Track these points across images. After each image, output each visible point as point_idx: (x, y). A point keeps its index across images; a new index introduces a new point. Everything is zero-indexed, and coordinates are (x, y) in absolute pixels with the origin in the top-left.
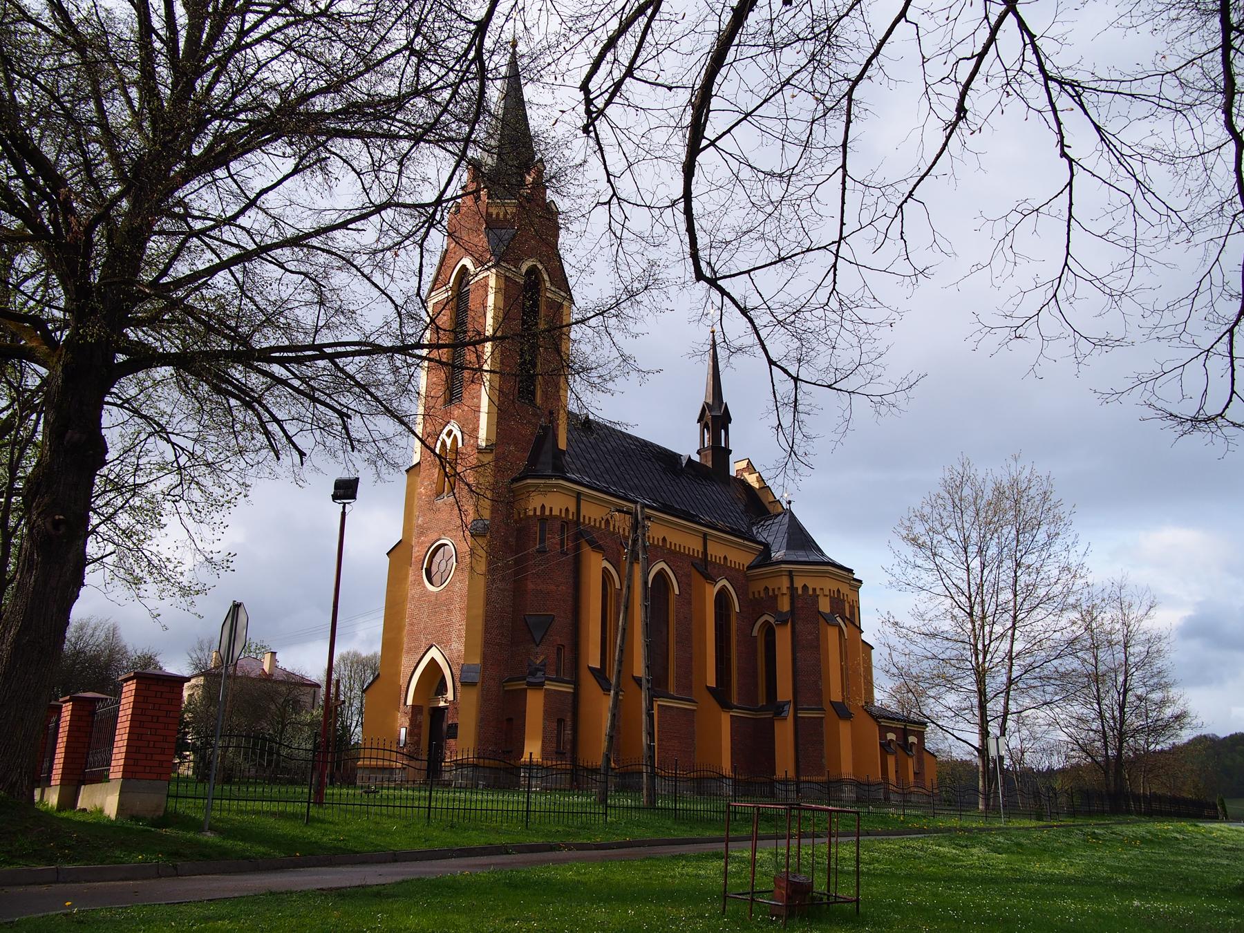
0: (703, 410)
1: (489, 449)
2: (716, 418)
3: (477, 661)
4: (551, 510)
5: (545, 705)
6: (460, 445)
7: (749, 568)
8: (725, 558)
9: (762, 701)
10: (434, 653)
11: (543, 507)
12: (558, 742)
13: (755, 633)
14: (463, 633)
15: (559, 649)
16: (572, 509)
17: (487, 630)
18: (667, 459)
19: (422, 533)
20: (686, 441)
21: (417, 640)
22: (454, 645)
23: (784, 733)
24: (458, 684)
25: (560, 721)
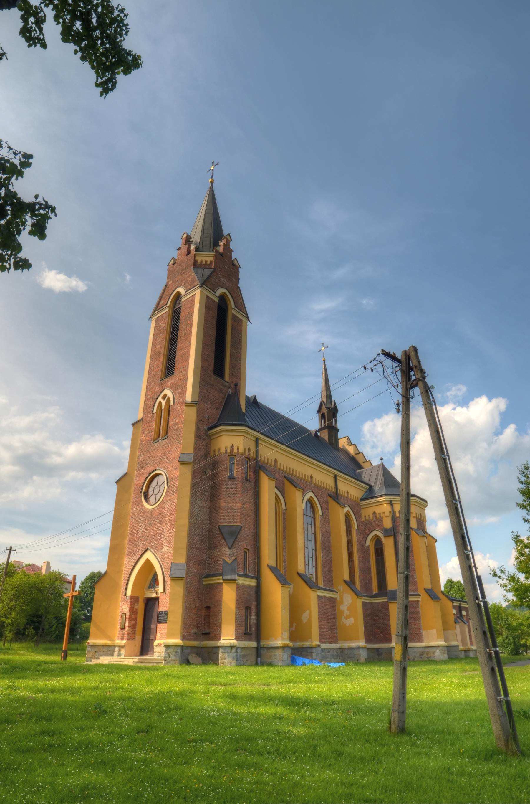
0: (321, 405)
1: (193, 403)
2: (329, 412)
3: (183, 560)
4: (238, 449)
5: (236, 597)
6: (172, 403)
7: (362, 500)
8: (347, 492)
9: (375, 591)
10: (149, 555)
11: (232, 446)
12: (246, 624)
13: (368, 543)
14: (172, 539)
15: (245, 552)
16: (253, 450)
17: (190, 537)
18: (302, 430)
19: (142, 467)
20: (311, 422)
21: (136, 545)
22: (165, 549)
23: (395, 612)
24: (168, 579)
25: (248, 608)
